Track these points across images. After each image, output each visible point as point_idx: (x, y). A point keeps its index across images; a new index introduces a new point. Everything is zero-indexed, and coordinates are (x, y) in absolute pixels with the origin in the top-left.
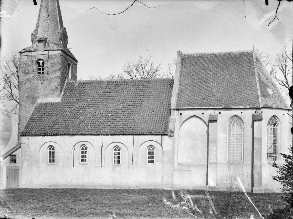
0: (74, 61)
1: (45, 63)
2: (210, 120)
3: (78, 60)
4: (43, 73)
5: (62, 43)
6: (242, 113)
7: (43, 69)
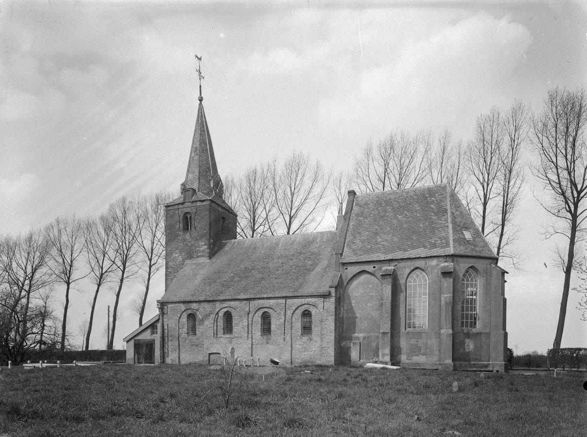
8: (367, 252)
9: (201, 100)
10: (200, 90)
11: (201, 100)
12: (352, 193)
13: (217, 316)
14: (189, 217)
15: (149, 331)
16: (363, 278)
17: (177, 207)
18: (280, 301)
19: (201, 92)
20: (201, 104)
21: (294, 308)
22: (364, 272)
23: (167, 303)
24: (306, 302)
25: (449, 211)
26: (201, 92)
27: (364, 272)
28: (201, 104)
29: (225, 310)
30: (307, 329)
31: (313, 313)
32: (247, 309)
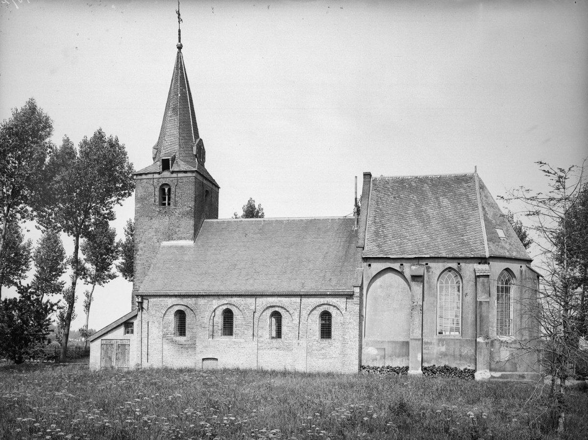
0: (214, 187)
1: (173, 189)
2: (86, 359)
3: (220, 186)
4: (169, 204)
5: (196, 161)
6: (402, 265)
7: (169, 199)
8: (403, 253)
9: (180, 48)
10: (179, 35)
11: (180, 48)
12: (367, 175)
13: (214, 314)
14: (166, 189)
15: (122, 330)
16: (389, 276)
17: (150, 176)
18: (294, 299)
19: (180, 38)
20: (179, 53)
21: (311, 309)
22: (390, 269)
23: (149, 296)
24: (326, 302)
25: (480, 206)
26: (180, 38)
27: (390, 269)
28: (179, 53)
29: (225, 307)
30: (326, 332)
31: (334, 315)
32: (253, 307)
